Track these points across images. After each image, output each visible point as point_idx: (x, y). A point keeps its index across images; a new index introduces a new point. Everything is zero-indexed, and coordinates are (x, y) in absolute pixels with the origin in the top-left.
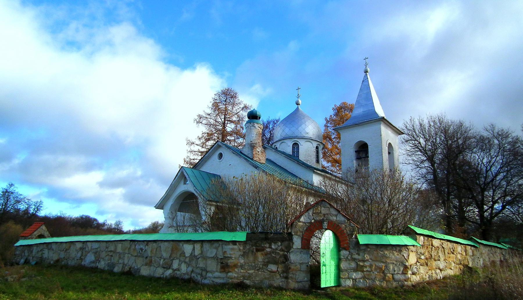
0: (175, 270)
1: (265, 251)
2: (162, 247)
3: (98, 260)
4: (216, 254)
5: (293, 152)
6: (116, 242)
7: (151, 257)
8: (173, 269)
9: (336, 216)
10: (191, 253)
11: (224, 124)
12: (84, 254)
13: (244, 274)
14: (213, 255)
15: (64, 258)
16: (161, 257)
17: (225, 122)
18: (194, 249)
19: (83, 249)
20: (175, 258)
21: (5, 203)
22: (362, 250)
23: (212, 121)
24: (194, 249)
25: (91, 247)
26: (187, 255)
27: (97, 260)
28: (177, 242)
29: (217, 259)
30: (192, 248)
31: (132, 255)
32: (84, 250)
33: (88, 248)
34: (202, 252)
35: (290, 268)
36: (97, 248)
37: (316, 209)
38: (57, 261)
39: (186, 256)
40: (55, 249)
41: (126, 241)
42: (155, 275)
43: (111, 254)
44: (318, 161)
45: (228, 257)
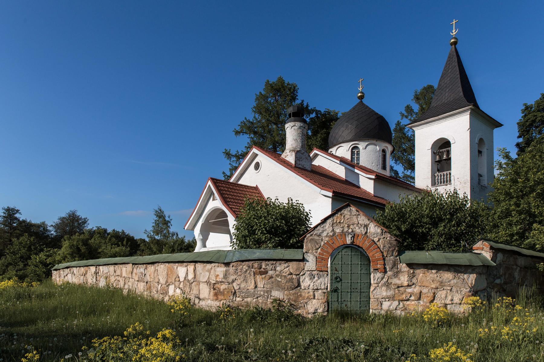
2: (158, 270)
4: (209, 278)
5: (352, 158)
10: (185, 277)
16: (158, 282)
20: (171, 283)
26: (182, 279)
28: (172, 264)
30: (186, 270)
32: (97, 275)
34: (195, 276)
36: (107, 273)
39: (181, 280)
44: (384, 168)
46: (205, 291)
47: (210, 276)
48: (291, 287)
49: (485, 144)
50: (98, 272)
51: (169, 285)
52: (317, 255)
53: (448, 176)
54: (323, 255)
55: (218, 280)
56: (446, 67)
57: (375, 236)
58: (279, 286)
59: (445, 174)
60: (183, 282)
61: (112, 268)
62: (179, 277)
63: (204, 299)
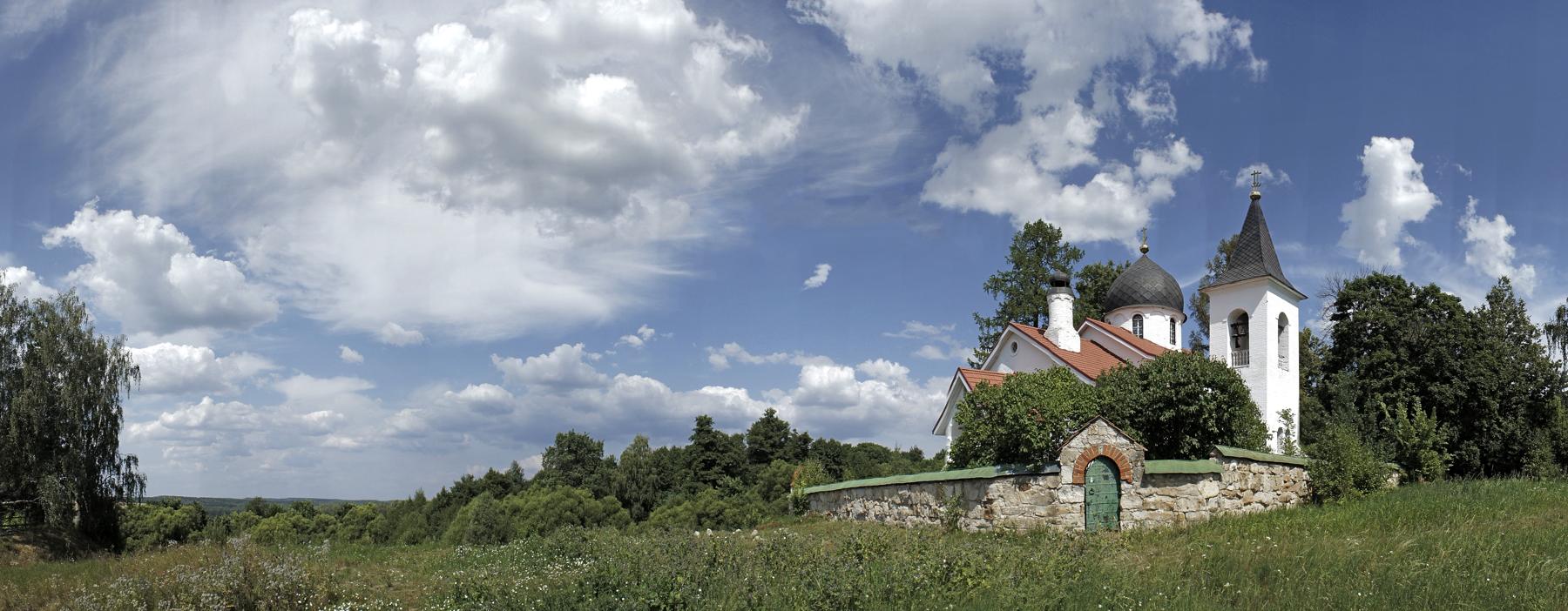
44: (1174, 342)
45: (992, 500)
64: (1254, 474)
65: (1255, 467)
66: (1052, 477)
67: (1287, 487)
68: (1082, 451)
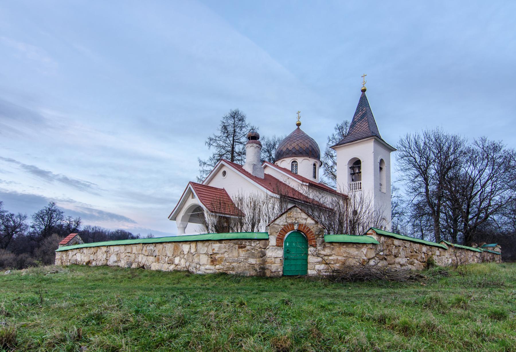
0: (177, 265)
1: (246, 248)
3: (119, 261)
4: (207, 251)
5: (292, 169)
6: (132, 245)
7: (159, 256)
8: (175, 264)
9: (306, 219)
11: (233, 145)
12: (108, 256)
13: (228, 266)
14: (205, 252)
15: (93, 259)
16: (166, 256)
17: (233, 143)
18: (190, 248)
19: (107, 252)
21: (50, 220)
22: (327, 247)
23: (221, 143)
24: (190, 248)
25: (114, 250)
26: (186, 253)
27: (118, 260)
28: (178, 243)
29: (208, 255)
31: (144, 255)
32: (108, 252)
33: (111, 250)
34: (196, 250)
35: (266, 261)
36: (118, 251)
37: (289, 214)
38: (89, 263)
39: (185, 253)
40: (86, 253)
41: (139, 244)
42: (162, 270)
43: (129, 254)
46: (204, 259)
47: (208, 250)
48: (261, 256)
49: (384, 163)
50: (109, 251)
51: (175, 257)
52: (276, 236)
53: (359, 185)
54: (280, 236)
55: (214, 252)
56: (357, 108)
57: (311, 225)
58: (253, 256)
59: (357, 183)
60: (187, 254)
61: (123, 248)
62: (183, 251)
63: (204, 265)
64: (396, 246)
65: (396, 242)
66: (263, 241)
67: (412, 256)
68: (283, 227)
